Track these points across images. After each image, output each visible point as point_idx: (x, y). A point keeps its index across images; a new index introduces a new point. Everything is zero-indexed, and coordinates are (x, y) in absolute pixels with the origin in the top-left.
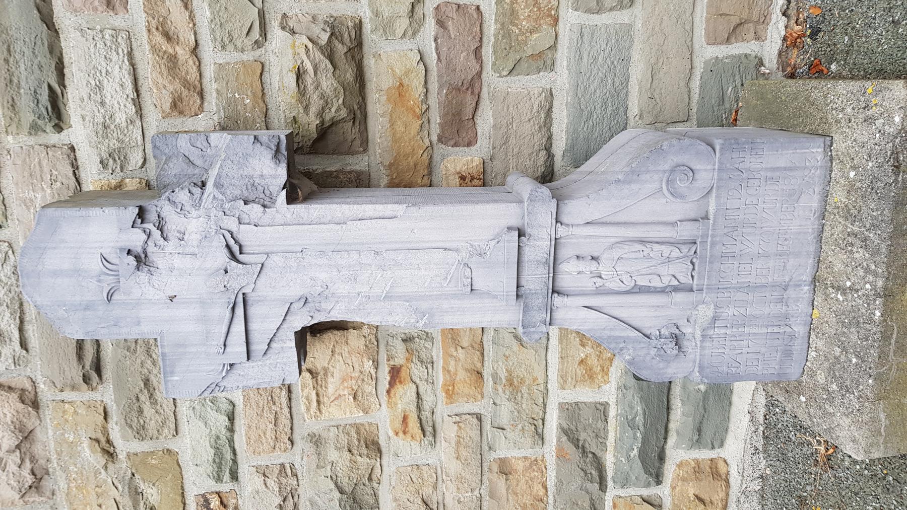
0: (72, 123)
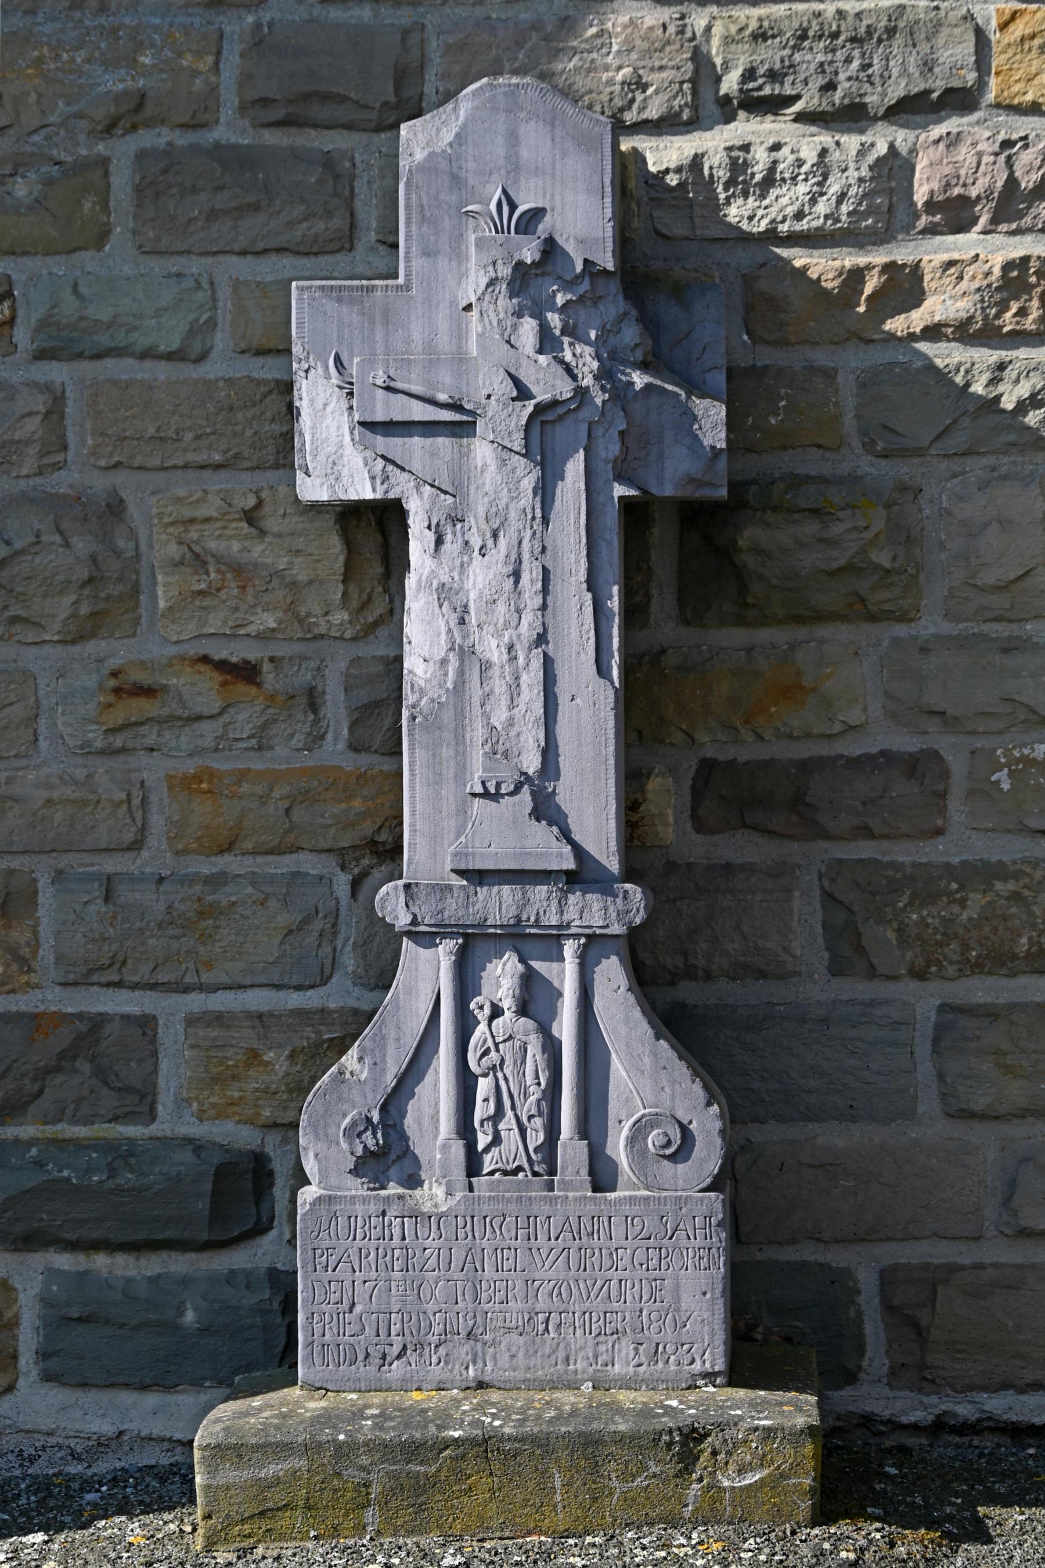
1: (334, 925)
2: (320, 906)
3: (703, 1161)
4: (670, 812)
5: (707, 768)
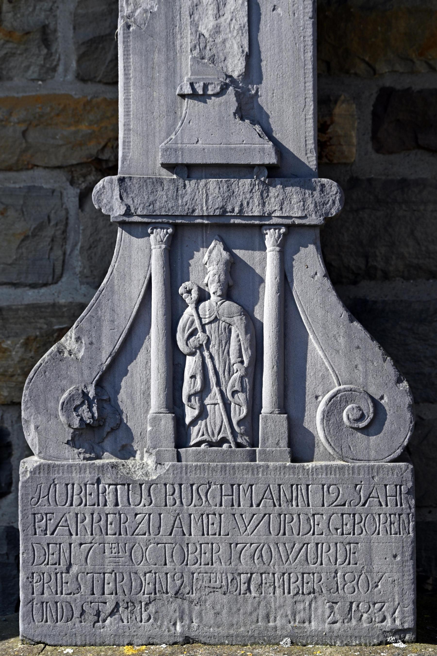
1: (64, 232)
2: (52, 216)
3: (393, 433)
4: (354, 134)
5: (386, 96)
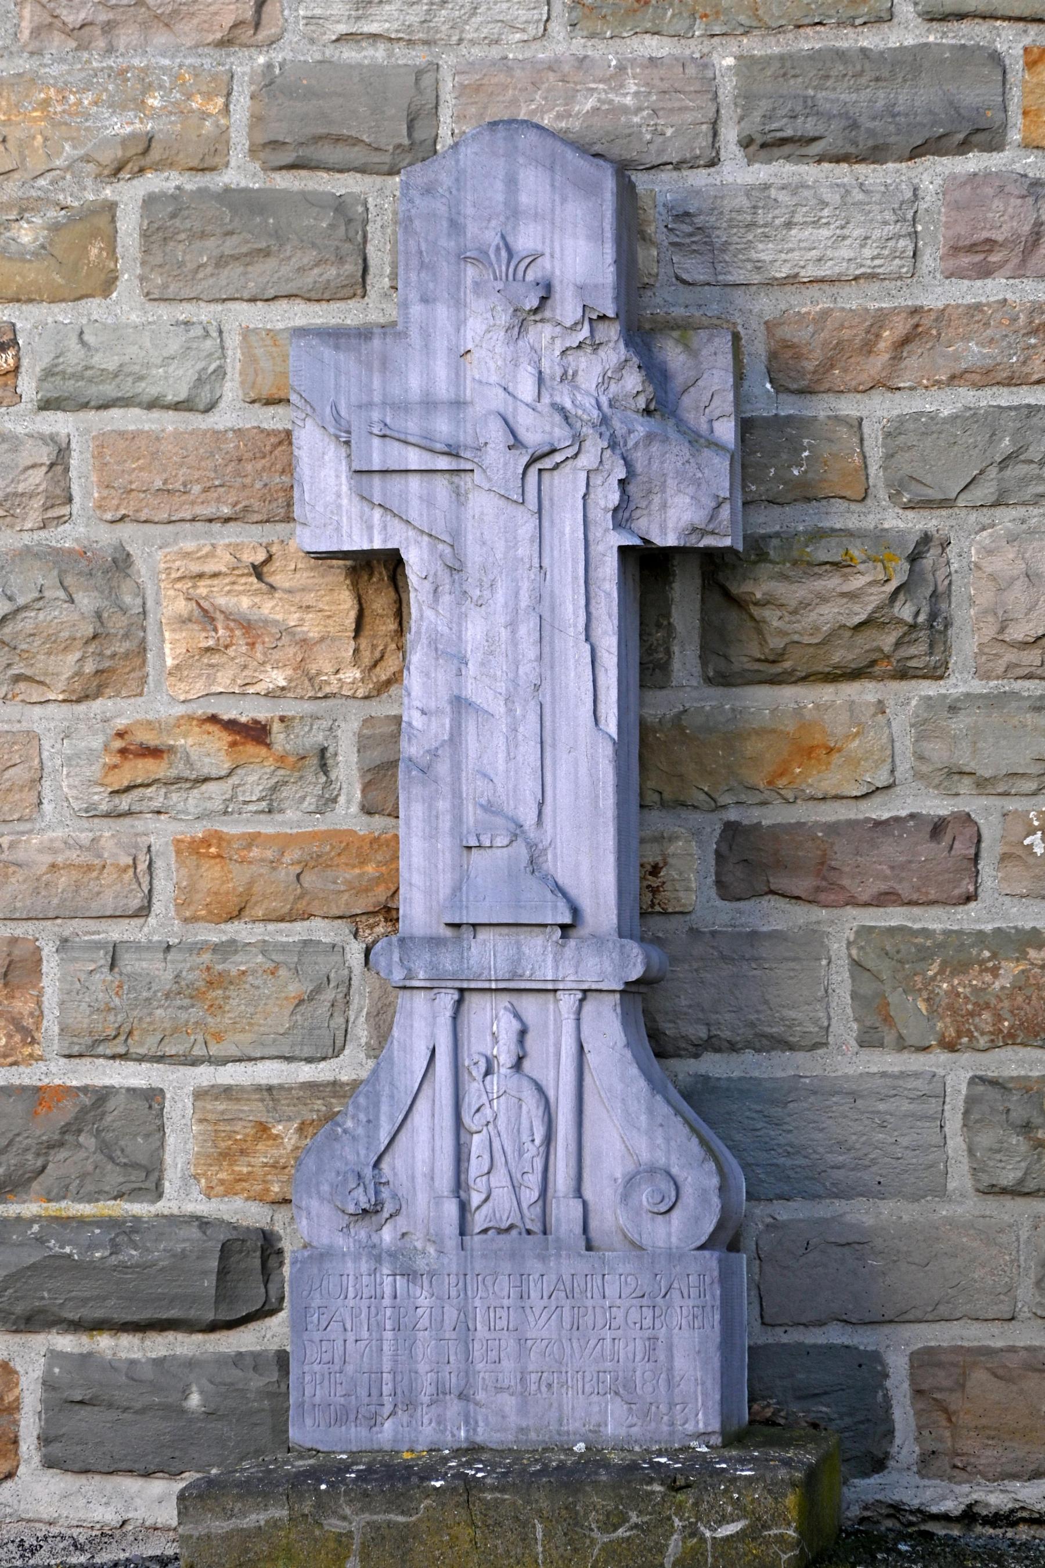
0: (757, 166)
1: (347, 994)
2: (332, 975)
